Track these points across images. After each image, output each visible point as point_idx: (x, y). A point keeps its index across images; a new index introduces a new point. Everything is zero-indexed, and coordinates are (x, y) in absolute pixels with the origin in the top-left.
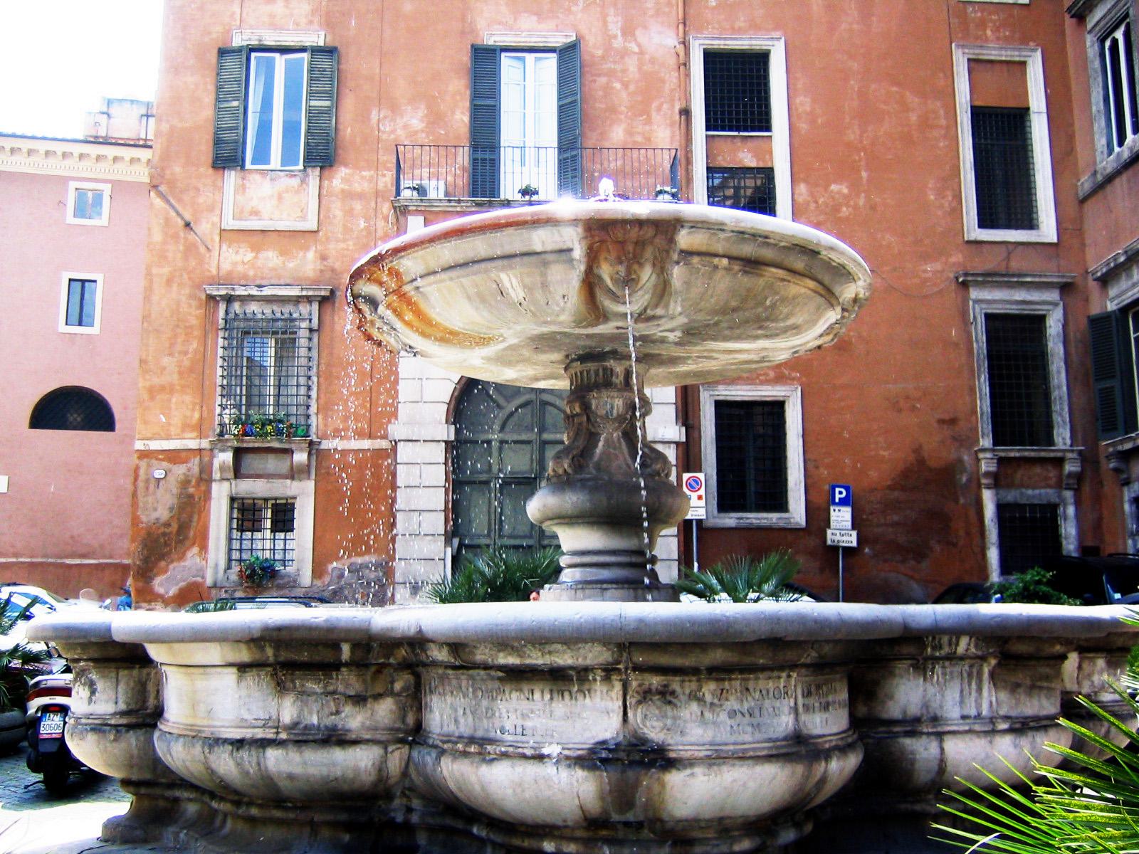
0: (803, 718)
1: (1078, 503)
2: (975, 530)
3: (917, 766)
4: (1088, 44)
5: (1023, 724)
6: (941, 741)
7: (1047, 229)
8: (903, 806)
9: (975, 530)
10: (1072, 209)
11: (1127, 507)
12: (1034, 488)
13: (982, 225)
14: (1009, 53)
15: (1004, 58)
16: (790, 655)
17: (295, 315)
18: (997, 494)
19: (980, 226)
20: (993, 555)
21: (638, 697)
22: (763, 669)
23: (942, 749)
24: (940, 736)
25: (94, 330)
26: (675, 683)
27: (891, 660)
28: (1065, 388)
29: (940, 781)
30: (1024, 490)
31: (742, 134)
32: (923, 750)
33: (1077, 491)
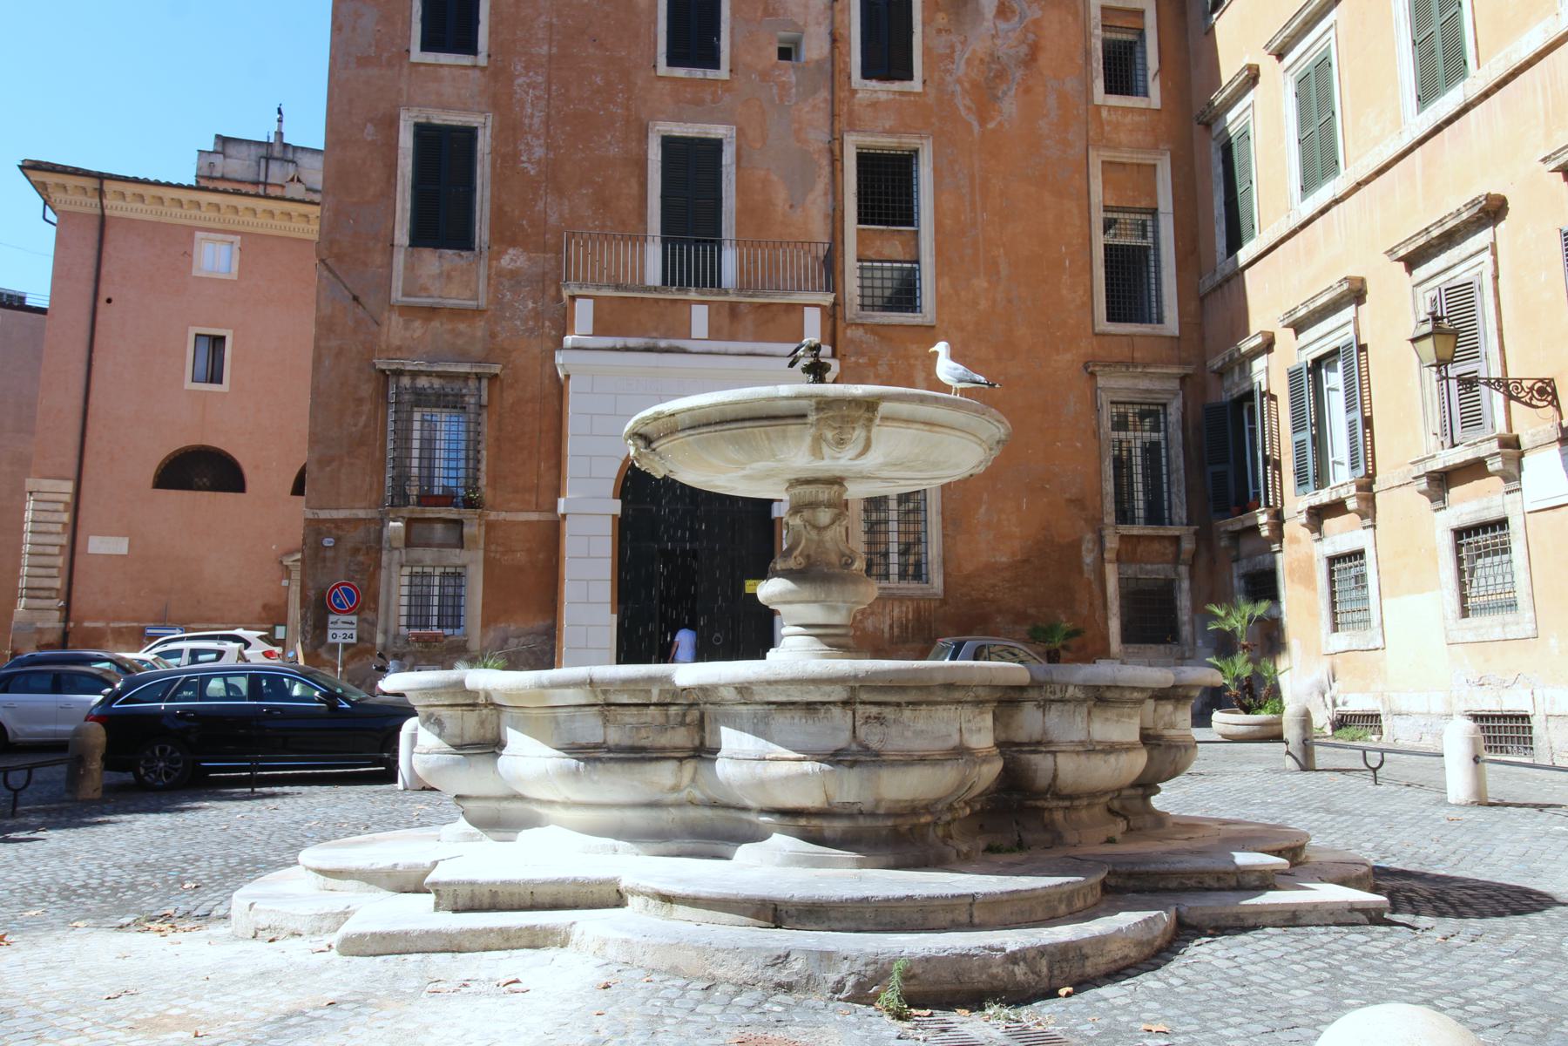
0: (966, 736)
1: (1192, 578)
2: (1098, 602)
3: (1039, 774)
4: (1213, 150)
5: (1111, 747)
6: (1055, 757)
7: (1171, 323)
8: (1029, 802)
9: (1098, 602)
10: (1193, 306)
11: (1236, 582)
12: (1152, 563)
13: (1111, 318)
14: (1140, 156)
15: (1135, 161)
16: (958, 695)
17: (464, 391)
18: (1118, 568)
19: (1108, 320)
20: (1114, 626)
21: (862, 721)
22: (940, 703)
23: (1055, 762)
24: (1054, 753)
25: (225, 387)
26: (888, 712)
27: (1020, 702)
28: (1182, 472)
29: (1054, 791)
30: (1143, 565)
31: (891, 228)
32: (1042, 764)
33: (1192, 567)
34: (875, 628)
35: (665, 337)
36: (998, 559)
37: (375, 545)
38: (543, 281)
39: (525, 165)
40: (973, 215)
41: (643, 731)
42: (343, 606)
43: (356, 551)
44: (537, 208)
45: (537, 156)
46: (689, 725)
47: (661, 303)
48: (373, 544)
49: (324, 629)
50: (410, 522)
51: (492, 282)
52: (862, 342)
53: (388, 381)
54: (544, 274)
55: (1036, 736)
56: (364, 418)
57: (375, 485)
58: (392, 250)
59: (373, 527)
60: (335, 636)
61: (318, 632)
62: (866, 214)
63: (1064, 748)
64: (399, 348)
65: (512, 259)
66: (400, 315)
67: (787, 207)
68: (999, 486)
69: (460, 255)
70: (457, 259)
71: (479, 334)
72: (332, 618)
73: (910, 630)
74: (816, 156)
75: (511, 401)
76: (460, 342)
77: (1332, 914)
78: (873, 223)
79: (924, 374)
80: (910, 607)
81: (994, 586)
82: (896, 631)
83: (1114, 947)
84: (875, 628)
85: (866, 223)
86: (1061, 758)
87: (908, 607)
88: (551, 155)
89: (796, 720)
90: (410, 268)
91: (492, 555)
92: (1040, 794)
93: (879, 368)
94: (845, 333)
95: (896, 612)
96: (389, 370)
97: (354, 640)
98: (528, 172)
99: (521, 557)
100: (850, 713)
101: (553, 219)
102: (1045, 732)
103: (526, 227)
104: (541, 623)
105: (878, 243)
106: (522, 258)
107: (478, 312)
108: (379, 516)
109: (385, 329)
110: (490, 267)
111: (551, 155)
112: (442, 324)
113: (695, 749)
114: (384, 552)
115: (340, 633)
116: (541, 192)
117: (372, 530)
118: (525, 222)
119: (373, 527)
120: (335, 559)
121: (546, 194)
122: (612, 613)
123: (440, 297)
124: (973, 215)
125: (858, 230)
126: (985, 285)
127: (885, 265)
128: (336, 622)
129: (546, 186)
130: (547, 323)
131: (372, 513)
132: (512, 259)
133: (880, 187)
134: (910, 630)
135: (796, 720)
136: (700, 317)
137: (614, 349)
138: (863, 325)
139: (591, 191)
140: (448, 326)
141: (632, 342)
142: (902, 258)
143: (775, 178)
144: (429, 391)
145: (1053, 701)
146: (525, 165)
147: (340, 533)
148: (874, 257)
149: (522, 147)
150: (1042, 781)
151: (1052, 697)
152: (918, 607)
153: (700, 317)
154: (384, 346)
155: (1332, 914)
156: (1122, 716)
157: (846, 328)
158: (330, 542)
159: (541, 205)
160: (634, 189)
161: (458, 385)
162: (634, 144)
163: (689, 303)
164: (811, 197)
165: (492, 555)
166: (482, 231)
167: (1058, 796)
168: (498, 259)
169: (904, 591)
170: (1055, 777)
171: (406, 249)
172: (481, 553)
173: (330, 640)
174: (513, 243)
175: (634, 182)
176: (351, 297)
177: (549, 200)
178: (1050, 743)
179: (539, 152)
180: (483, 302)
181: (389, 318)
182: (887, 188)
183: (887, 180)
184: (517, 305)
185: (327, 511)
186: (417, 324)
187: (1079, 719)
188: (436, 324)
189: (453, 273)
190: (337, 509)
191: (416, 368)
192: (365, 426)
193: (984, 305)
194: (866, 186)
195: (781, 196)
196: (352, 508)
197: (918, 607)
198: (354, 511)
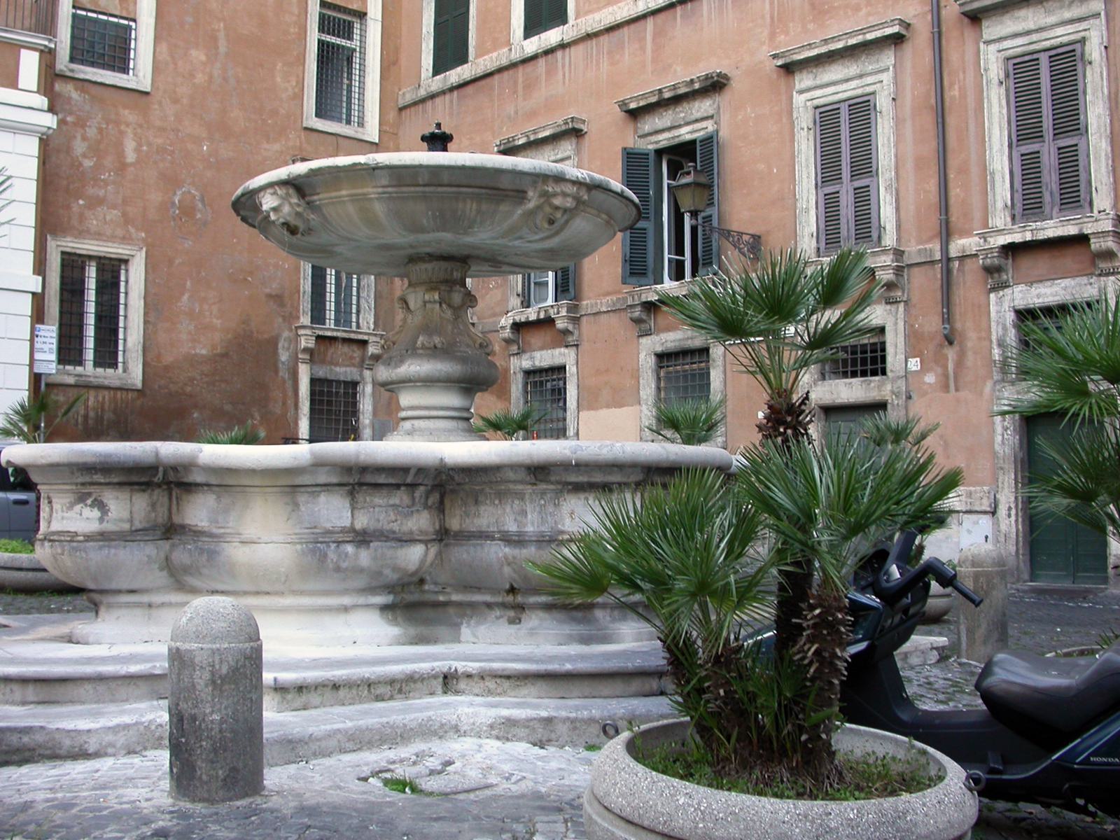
36: (198, 351)
81: (192, 379)
126: (203, 58)
142: (117, 13)
193: (200, 78)
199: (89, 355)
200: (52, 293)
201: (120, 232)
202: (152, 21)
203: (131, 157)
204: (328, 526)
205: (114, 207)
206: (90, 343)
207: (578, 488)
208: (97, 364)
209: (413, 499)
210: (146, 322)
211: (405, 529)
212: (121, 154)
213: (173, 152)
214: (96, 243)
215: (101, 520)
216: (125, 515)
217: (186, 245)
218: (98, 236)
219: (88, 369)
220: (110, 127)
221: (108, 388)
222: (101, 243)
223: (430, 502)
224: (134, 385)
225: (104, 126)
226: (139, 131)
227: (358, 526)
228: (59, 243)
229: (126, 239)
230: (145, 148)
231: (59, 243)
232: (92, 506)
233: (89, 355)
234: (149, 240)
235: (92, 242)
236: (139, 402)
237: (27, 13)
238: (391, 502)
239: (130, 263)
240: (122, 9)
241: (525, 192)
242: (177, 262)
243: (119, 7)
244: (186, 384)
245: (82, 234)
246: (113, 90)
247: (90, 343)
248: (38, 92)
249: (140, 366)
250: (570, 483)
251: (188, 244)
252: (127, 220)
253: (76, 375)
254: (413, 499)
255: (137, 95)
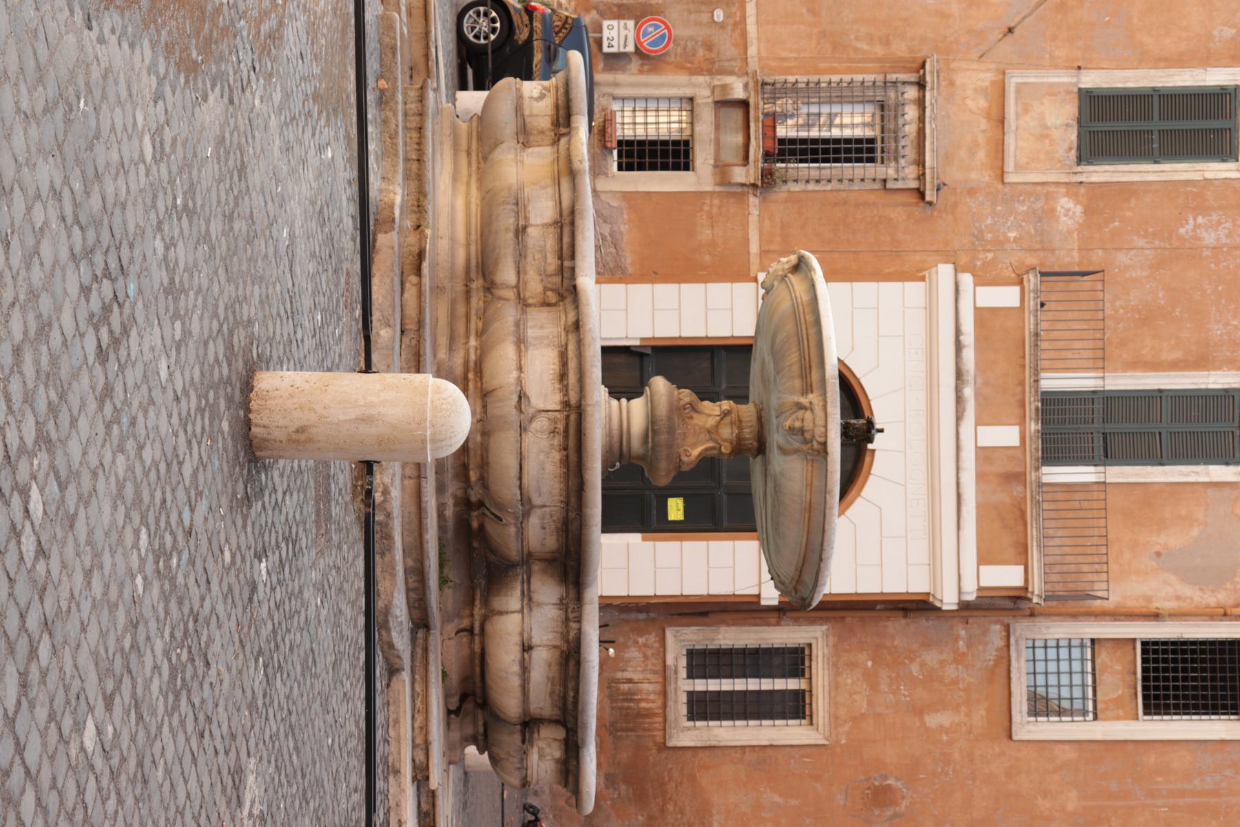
3: (504, 599)
24: (522, 611)
34: (629, 660)
35: (977, 395)
36: (716, 818)
37: (712, 67)
38: (1043, 249)
39: (1191, 222)
40: (1164, 792)
41: (540, 256)
42: (644, 36)
43: (709, 47)
44: (1135, 238)
45: (1204, 235)
46: (545, 294)
47: (1019, 389)
48: (717, 64)
49: (618, 17)
50: (744, 104)
51: (1039, 188)
52: (986, 644)
53: (911, 72)
54: (1053, 250)
55: (536, 597)
56: (866, 47)
57: (785, 64)
58: (1072, 68)
59: (737, 65)
60: (610, 28)
61: (615, 9)
62: (1155, 652)
63: (526, 620)
64: (951, 83)
65: (1069, 210)
66: (993, 83)
67: (1158, 548)
68: (808, 821)
69: (1070, 149)
70: (1066, 146)
71: (974, 175)
72: (631, 23)
73: (626, 704)
74: (1229, 586)
75: (893, 216)
76: (962, 153)
77: (397, 805)
78: (1144, 661)
79: (947, 723)
80: (655, 705)
81: (682, 812)
82: (625, 687)
83: (387, 583)
84: (629, 660)
85: (1144, 651)
86: (517, 617)
87: (653, 702)
88: (1206, 253)
89: (552, 367)
90: (1052, 91)
91: (708, 201)
92: (486, 602)
93: (954, 666)
94: (996, 622)
95: (646, 687)
96: (924, 74)
97: (606, 49)
98: (1182, 226)
99: (706, 234)
100: (558, 408)
101: (1122, 258)
102: (539, 605)
103: (1111, 226)
104: (629, 261)
105: (1118, 667)
106: (1070, 222)
107: (1002, 174)
108: (749, 71)
109: (975, 66)
110: (1057, 184)
111: (1206, 253)
112: (984, 131)
113: (525, 300)
114: (707, 78)
115: (614, 33)
116: (1157, 243)
117: (734, 64)
118: (1116, 224)
119: (737, 65)
120: (698, 24)
121: (1155, 249)
122: (642, 339)
123: (1017, 129)
124: (1164, 792)
125: (1134, 640)
126: (1070, 807)
127: (1089, 664)
128: (626, 28)
129: (1165, 249)
130: (990, 256)
131: (753, 65)
132: (1068, 210)
133: (1194, 670)
134: (626, 704)
135: (552, 367)
136: (1006, 436)
137: (958, 332)
138: (1008, 646)
139: (1163, 302)
140: (981, 139)
141: (969, 355)
142: (1099, 697)
143: (1195, 532)
144: (901, 121)
145: (566, 611)
146: (1191, 222)
147: (729, 28)
148: (1098, 661)
149: (1215, 217)
150: (498, 603)
151: (569, 610)
152: (654, 715)
153: (1006, 436)
154: (954, 65)
155: (397, 805)
156: (553, 685)
157: (1002, 624)
158: (718, 16)
159: (1141, 243)
160: (1167, 356)
161: (910, 153)
162: (1228, 354)
163: (1022, 422)
164: (1172, 578)
165: (708, 201)
166: (1102, 173)
167: (485, 619)
168: (1068, 195)
169: (673, 696)
170: (501, 613)
171: (1075, 84)
172: (709, 188)
173: (606, 23)
174: (1088, 211)
175: (1177, 355)
176: (1012, 25)
177: (1147, 252)
178: (531, 609)
179: (1209, 238)
180: (1010, 178)
181: (989, 70)
182: (1194, 679)
183: (1204, 679)
184: (1012, 218)
185: (754, 12)
186: (983, 103)
187: (550, 636)
188: (984, 124)
189: (1047, 141)
190: (757, 22)
191: (927, 104)
192: (856, 50)
193: (1044, 804)
194: (1193, 652)
195: (1172, 539)
196: (759, 40)
197: (654, 715)
198: (755, 42)
199: (700, 685)
200: (765, 635)
201: (842, 712)
202: (1099, 736)
203: (934, 720)
204: (530, 208)
205: (870, 703)
206: (713, 685)
207: (563, 357)
208: (690, 694)
209: (551, 276)
210: (743, 747)
211: (528, 268)
212: (932, 708)
213: (947, 774)
214: (826, 683)
215: (531, 98)
216: (535, 112)
217: (839, 797)
218: (835, 687)
219: (684, 685)
220: (962, 693)
221: (665, 706)
222: (827, 688)
223: (549, 293)
224: (670, 737)
225: (961, 686)
226: (964, 729)
227: (529, 230)
228: (820, 640)
229: (834, 718)
230: (945, 738)
231: (820, 640)
232: (541, 93)
233: (700, 685)
234: (838, 750)
235: (826, 679)
236: (651, 744)
237: (1071, 586)
238: (549, 255)
239: (810, 727)
240: (1106, 702)
241: (812, 392)
242: (818, 786)
243: (1107, 698)
244: (675, 805)
245: (836, 668)
246: (1006, 693)
247: (713, 685)
248: (980, 589)
249: (692, 744)
250: (566, 349)
251: (840, 799)
252: (856, 719)
253: (676, 667)
254: (551, 276)
255: (1006, 724)
